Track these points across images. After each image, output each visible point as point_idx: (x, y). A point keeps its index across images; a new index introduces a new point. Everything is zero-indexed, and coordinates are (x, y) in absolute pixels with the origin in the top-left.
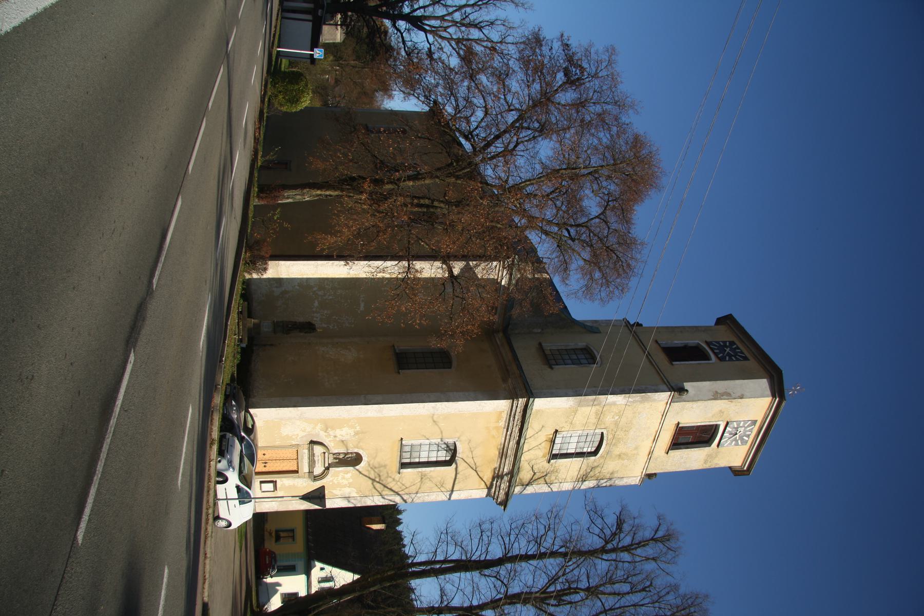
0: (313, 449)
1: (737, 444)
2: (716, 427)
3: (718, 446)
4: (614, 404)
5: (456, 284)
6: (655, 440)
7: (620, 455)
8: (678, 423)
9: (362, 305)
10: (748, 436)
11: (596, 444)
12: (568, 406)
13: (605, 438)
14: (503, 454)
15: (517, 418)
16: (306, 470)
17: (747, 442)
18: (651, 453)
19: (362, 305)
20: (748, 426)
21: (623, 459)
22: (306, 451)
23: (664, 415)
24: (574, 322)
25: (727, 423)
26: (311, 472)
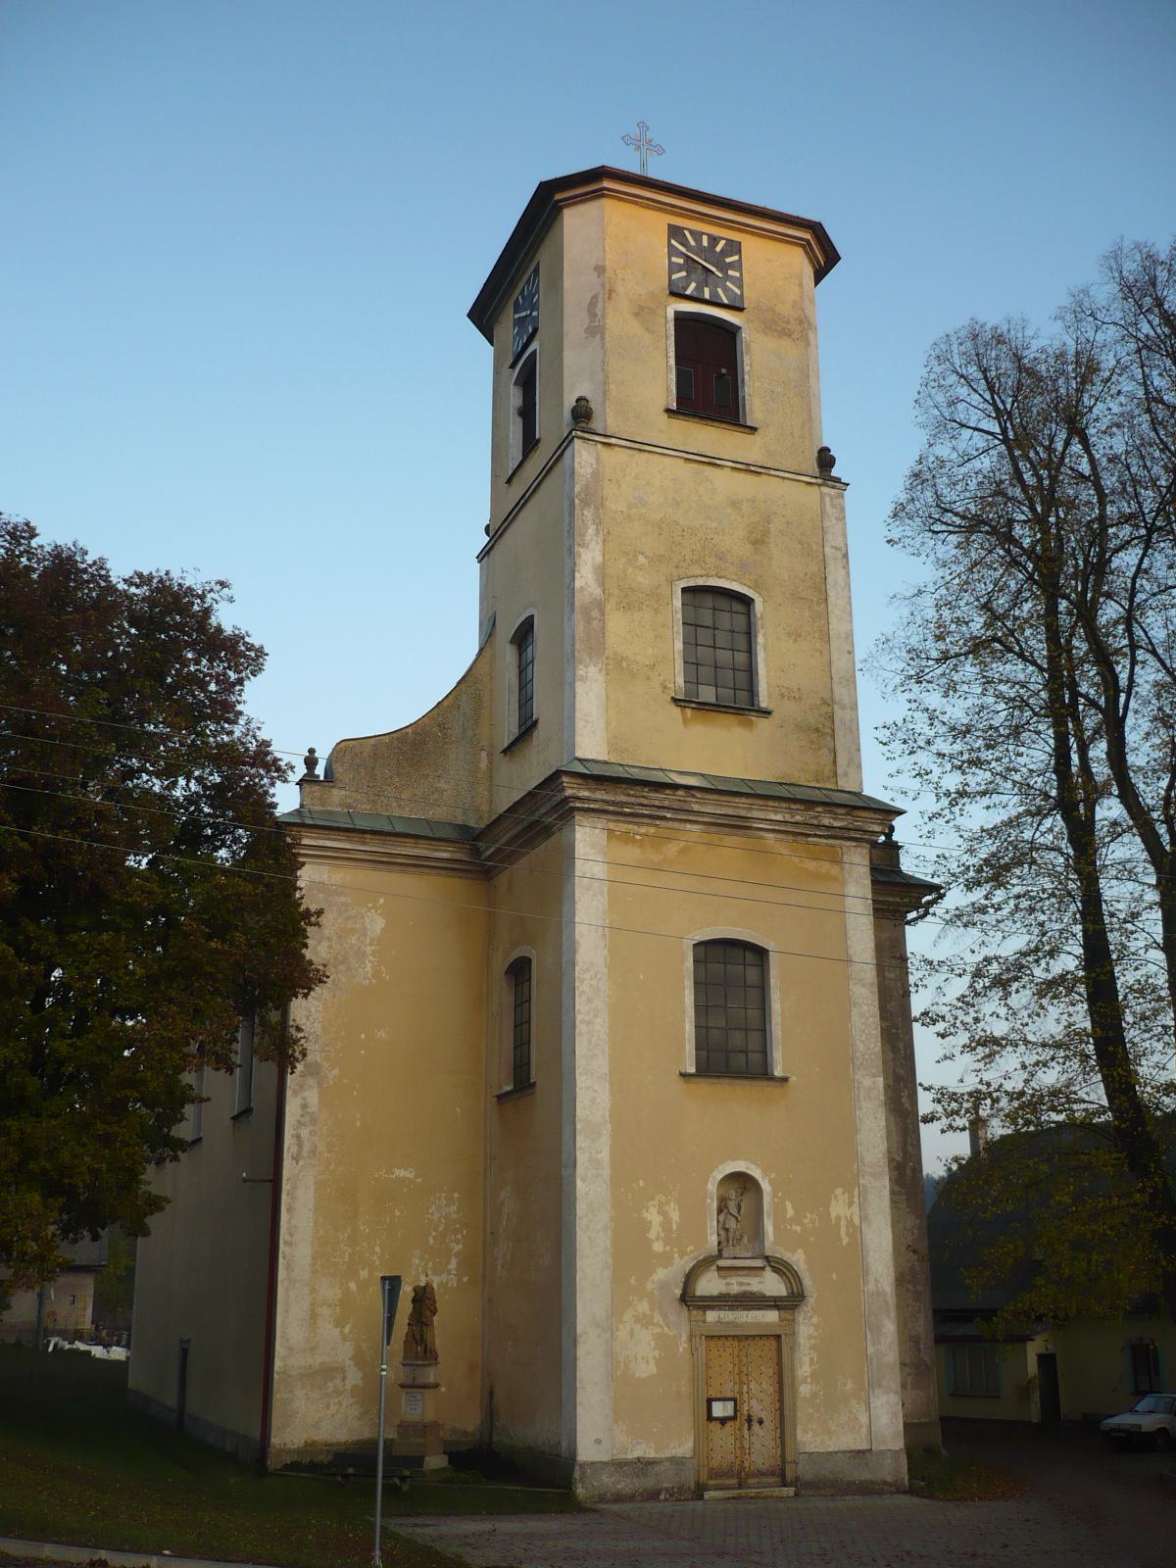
0: (703, 1298)
1: (738, 265)
2: (681, 319)
3: (740, 309)
4: (601, 573)
5: (1049, 1053)
6: (712, 462)
7: (755, 543)
8: (668, 411)
9: (401, 1173)
10: (714, 240)
11: (723, 603)
12: (601, 678)
13: (701, 582)
14: (738, 825)
15: (623, 798)
16: (772, 1316)
17: (730, 242)
18: (748, 469)
19: (401, 1173)
20: (685, 244)
21: (766, 533)
22: (712, 1316)
23: (638, 446)
24: (901, 872)
25: (673, 294)
26: (775, 1303)
